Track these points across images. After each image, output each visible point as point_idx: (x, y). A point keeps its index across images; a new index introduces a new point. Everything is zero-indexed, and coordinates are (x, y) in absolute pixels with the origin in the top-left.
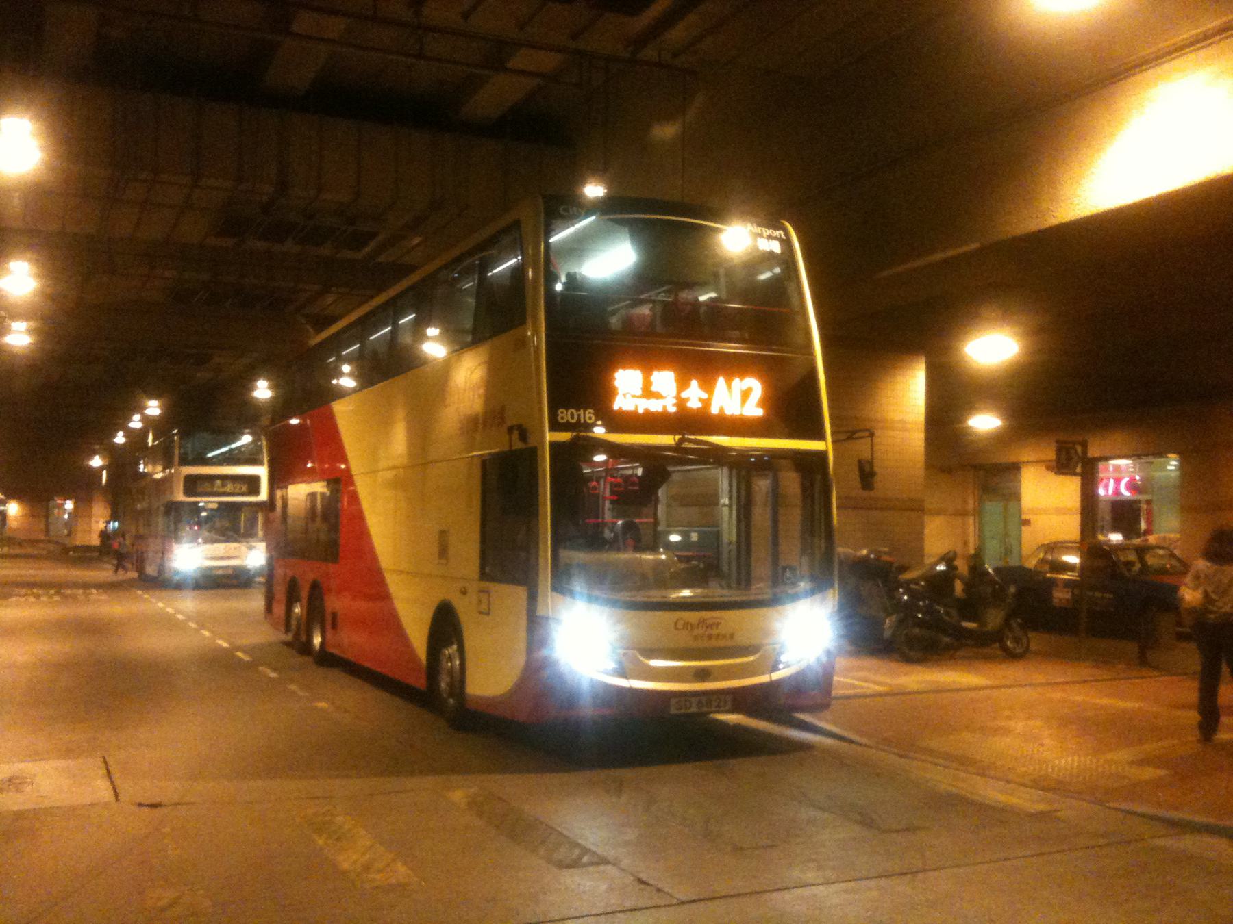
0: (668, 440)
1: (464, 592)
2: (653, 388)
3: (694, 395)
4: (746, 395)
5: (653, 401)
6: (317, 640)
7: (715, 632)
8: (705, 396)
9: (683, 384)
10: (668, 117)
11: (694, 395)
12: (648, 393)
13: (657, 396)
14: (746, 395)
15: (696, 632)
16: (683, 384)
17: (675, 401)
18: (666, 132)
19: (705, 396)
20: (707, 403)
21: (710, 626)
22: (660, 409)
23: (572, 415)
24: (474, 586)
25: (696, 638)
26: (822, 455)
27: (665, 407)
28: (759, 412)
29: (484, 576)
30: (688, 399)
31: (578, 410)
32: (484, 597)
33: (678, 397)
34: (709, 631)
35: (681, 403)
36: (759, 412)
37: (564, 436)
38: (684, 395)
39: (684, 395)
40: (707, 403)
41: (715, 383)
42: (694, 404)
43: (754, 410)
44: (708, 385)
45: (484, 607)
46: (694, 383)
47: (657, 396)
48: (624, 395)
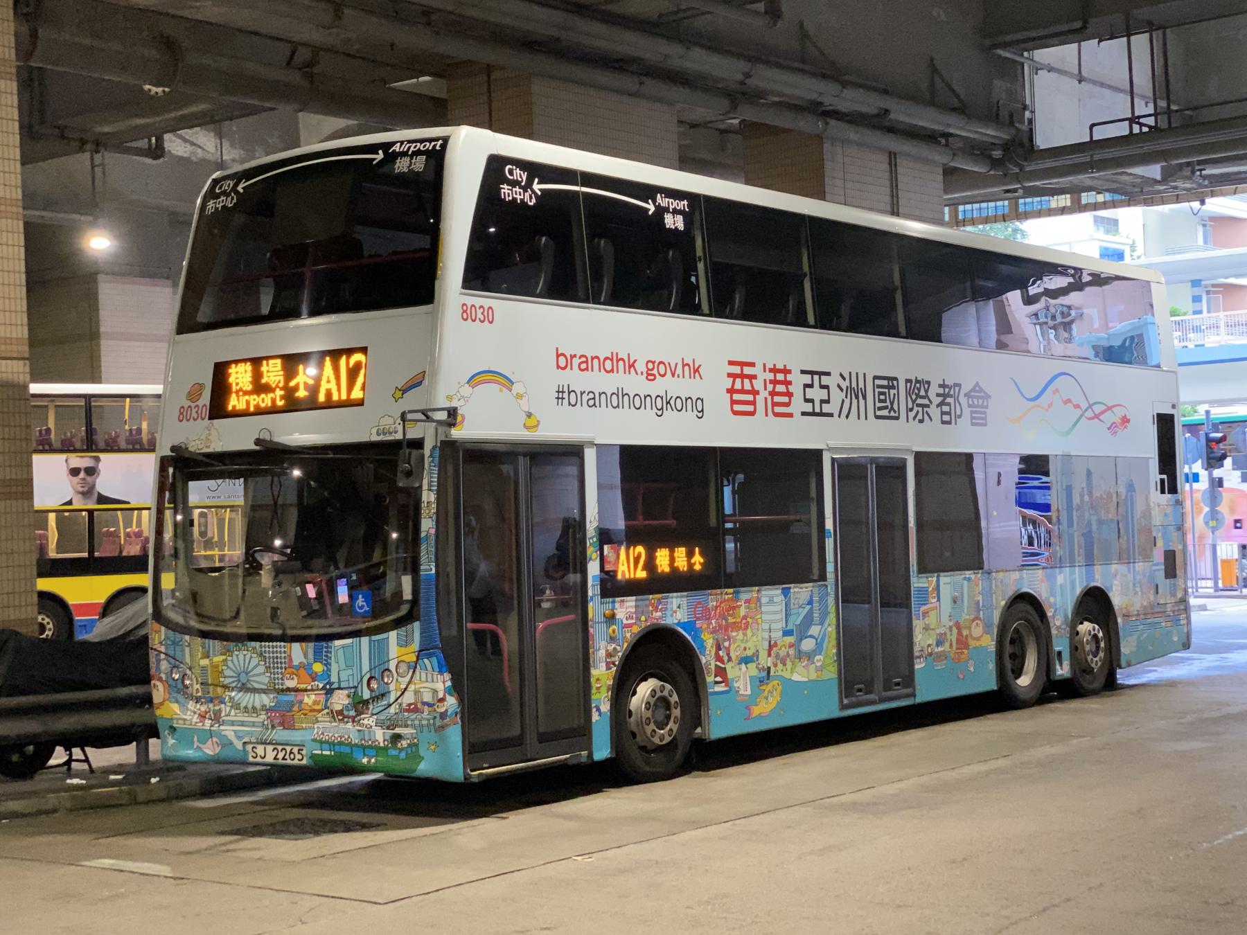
12: (260, 387)
17: (282, 393)
30: (296, 388)
33: (286, 388)
38: (292, 384)
48: (237, 392)
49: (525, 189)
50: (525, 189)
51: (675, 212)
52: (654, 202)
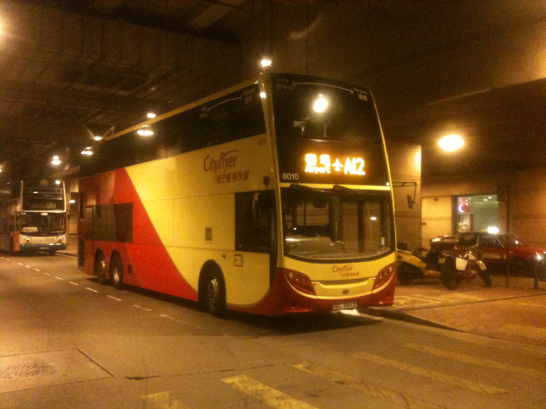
0: (330, 186)
1: (224, 256)
2: (321, 162)
3: (338, 166)
4: (358, 165)
5: (321, 168)
6: (116, 277)
7: (350, 272)
8: (342, 166)
9: (333, 161)
10: (299, 29)
11: (338, 166)
12: (319, 165)
13: (322, 166)
14: (358, 165)
15: (342, 272)
16: (333, 161)
17: (330, 168)
18: (297, 36)
19: (342, 166)
20: (342, 169)
21: (349, 269)
22: (324, 172)
23: (289, 176)
24: (231, 255)
25: (342, 275)
26: (388, 193)
27: (326, 171)
28: (363, 173)
29: (237, 248)
31: (291, 174)
32: (238, 258)
34: (348, 272)
35: (332, 169)
36: (363, 173)
37: (287, 185)
39: (333, 165)
40: (342, 169)
41: (345, 161)
42: (338, 170)
43: (361, 172)
44: (343, 162)
45: (239, 262)
46: (337, 160)
47: (322, 166)
49: (288, 85)
50: (288, 85)
51: (363, 94)
52: (353, 90)
